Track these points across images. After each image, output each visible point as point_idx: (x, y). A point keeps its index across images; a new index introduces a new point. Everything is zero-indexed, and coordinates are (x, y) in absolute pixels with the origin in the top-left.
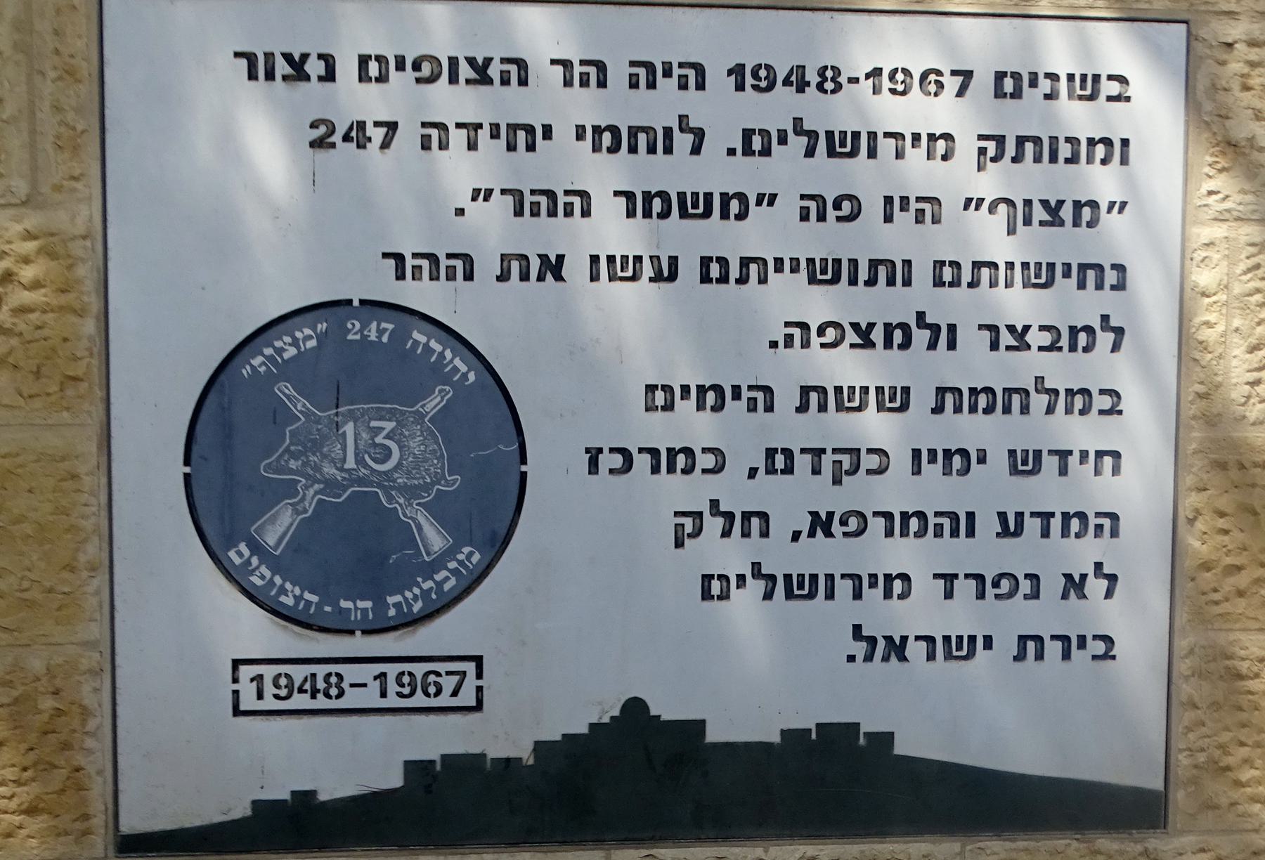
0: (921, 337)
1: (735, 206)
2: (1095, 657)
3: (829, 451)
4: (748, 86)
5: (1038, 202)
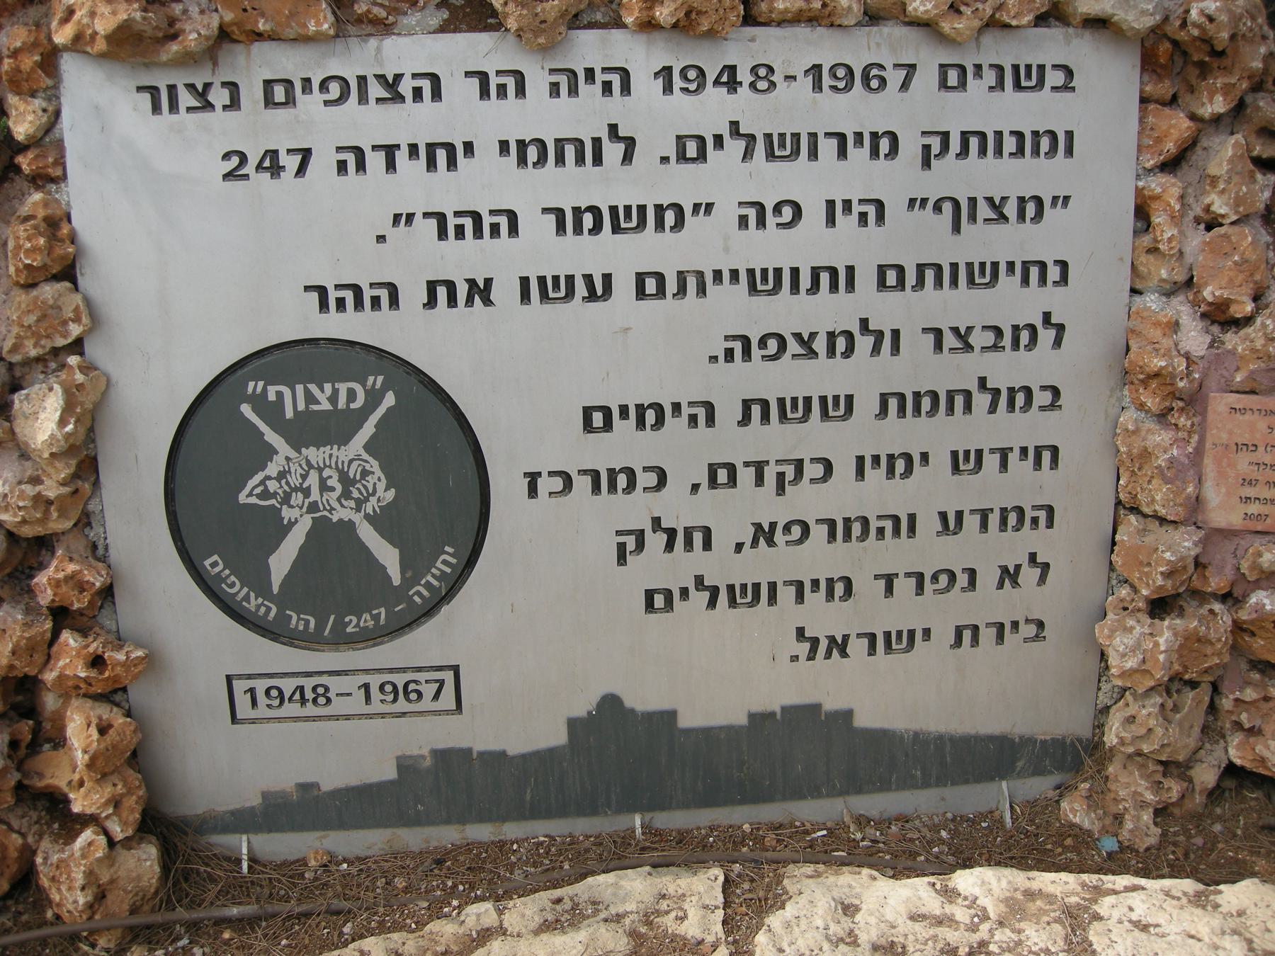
0: (864, 344)
1: (670, 217)
2: (1026, 640)
3: (772, 463)
4: (676, 88)
5: (983, 200)
